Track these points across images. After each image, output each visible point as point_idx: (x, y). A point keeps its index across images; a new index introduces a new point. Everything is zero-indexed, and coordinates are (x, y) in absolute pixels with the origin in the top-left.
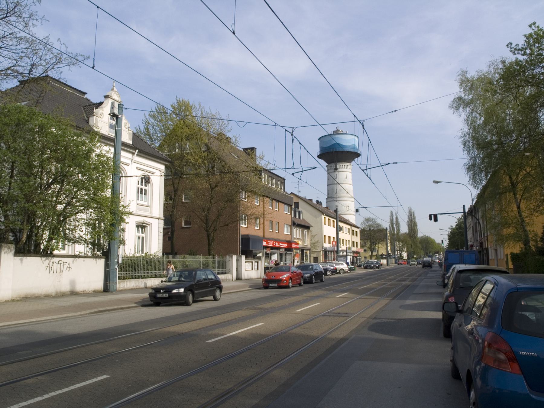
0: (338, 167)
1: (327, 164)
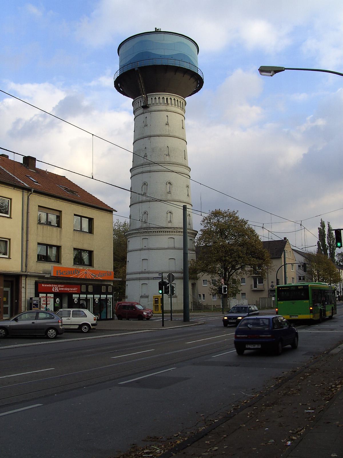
0: (149, 102)
1: (132, 100)
